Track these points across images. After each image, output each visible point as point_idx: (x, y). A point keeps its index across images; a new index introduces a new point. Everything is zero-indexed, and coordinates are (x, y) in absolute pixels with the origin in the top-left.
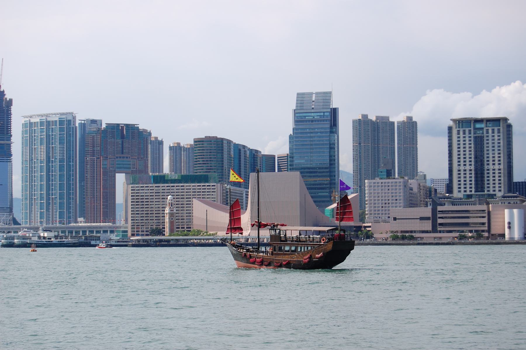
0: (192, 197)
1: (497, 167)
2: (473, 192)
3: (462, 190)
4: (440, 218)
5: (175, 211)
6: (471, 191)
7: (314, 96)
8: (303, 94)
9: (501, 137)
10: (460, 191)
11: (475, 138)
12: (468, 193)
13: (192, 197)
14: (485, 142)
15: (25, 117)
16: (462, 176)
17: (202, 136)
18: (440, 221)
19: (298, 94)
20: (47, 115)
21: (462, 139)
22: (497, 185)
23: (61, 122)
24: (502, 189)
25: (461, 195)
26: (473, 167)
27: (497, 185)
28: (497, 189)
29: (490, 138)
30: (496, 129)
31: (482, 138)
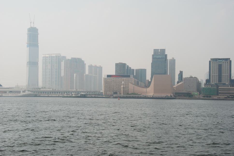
0: (122, 81)
1: (226, 74)
2: (218, 83)
3: (214, 82)
4: (219, 91)
5: (125, 87)
6: (217, 82)
7: (159, 50)
8: (156, 50)
9: (228, 65)
10: (213, 82)
11: (219, 65)
12: (216, 83)
13: (122, 81)
14: (222, 66)
15: (43, 55)
16: (214, 77)
17: (118, 62)
18: (219, 92)
19: (154, 49)
20: (51, 54)
21: (214, 65)
22: (226, 80)
23: (56, 57)
24: (228, 82)
25: (213, 83)
26: (218, 74)
27: (226, 80)
28: (226, 82)
29: (224, 65)
30: (216, 62)
31: (221, 65)
